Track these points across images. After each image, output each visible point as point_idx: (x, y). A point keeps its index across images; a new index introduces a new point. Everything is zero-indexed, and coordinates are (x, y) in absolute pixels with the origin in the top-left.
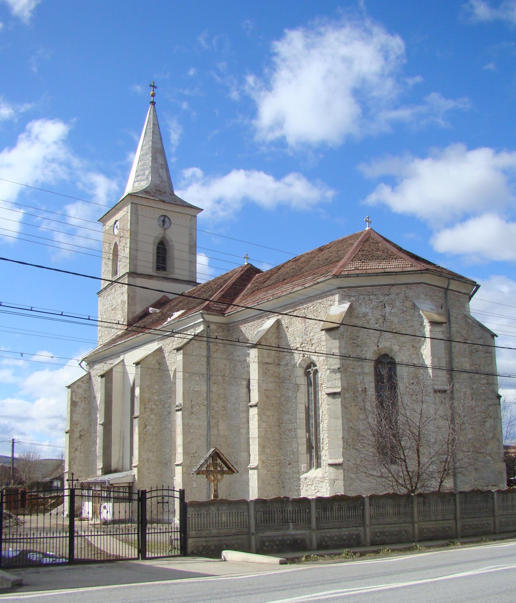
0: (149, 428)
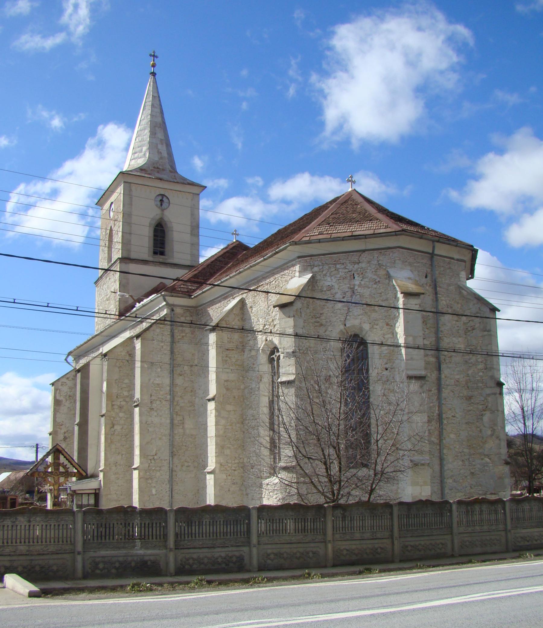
0: (118, 428)
